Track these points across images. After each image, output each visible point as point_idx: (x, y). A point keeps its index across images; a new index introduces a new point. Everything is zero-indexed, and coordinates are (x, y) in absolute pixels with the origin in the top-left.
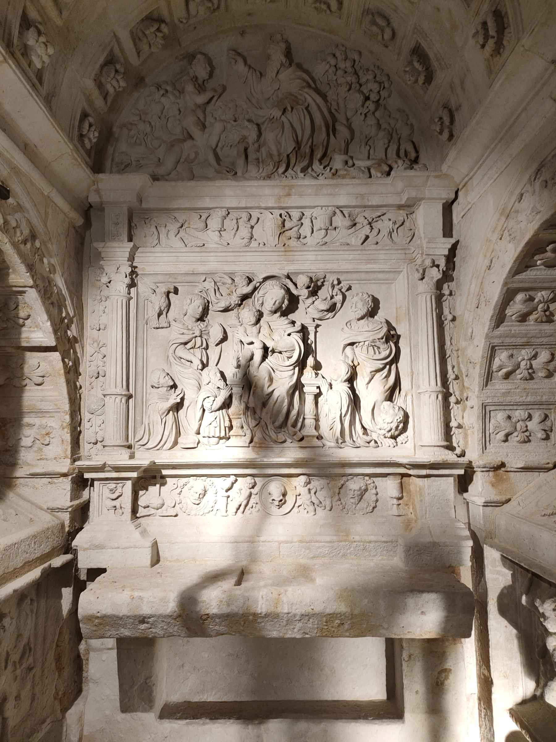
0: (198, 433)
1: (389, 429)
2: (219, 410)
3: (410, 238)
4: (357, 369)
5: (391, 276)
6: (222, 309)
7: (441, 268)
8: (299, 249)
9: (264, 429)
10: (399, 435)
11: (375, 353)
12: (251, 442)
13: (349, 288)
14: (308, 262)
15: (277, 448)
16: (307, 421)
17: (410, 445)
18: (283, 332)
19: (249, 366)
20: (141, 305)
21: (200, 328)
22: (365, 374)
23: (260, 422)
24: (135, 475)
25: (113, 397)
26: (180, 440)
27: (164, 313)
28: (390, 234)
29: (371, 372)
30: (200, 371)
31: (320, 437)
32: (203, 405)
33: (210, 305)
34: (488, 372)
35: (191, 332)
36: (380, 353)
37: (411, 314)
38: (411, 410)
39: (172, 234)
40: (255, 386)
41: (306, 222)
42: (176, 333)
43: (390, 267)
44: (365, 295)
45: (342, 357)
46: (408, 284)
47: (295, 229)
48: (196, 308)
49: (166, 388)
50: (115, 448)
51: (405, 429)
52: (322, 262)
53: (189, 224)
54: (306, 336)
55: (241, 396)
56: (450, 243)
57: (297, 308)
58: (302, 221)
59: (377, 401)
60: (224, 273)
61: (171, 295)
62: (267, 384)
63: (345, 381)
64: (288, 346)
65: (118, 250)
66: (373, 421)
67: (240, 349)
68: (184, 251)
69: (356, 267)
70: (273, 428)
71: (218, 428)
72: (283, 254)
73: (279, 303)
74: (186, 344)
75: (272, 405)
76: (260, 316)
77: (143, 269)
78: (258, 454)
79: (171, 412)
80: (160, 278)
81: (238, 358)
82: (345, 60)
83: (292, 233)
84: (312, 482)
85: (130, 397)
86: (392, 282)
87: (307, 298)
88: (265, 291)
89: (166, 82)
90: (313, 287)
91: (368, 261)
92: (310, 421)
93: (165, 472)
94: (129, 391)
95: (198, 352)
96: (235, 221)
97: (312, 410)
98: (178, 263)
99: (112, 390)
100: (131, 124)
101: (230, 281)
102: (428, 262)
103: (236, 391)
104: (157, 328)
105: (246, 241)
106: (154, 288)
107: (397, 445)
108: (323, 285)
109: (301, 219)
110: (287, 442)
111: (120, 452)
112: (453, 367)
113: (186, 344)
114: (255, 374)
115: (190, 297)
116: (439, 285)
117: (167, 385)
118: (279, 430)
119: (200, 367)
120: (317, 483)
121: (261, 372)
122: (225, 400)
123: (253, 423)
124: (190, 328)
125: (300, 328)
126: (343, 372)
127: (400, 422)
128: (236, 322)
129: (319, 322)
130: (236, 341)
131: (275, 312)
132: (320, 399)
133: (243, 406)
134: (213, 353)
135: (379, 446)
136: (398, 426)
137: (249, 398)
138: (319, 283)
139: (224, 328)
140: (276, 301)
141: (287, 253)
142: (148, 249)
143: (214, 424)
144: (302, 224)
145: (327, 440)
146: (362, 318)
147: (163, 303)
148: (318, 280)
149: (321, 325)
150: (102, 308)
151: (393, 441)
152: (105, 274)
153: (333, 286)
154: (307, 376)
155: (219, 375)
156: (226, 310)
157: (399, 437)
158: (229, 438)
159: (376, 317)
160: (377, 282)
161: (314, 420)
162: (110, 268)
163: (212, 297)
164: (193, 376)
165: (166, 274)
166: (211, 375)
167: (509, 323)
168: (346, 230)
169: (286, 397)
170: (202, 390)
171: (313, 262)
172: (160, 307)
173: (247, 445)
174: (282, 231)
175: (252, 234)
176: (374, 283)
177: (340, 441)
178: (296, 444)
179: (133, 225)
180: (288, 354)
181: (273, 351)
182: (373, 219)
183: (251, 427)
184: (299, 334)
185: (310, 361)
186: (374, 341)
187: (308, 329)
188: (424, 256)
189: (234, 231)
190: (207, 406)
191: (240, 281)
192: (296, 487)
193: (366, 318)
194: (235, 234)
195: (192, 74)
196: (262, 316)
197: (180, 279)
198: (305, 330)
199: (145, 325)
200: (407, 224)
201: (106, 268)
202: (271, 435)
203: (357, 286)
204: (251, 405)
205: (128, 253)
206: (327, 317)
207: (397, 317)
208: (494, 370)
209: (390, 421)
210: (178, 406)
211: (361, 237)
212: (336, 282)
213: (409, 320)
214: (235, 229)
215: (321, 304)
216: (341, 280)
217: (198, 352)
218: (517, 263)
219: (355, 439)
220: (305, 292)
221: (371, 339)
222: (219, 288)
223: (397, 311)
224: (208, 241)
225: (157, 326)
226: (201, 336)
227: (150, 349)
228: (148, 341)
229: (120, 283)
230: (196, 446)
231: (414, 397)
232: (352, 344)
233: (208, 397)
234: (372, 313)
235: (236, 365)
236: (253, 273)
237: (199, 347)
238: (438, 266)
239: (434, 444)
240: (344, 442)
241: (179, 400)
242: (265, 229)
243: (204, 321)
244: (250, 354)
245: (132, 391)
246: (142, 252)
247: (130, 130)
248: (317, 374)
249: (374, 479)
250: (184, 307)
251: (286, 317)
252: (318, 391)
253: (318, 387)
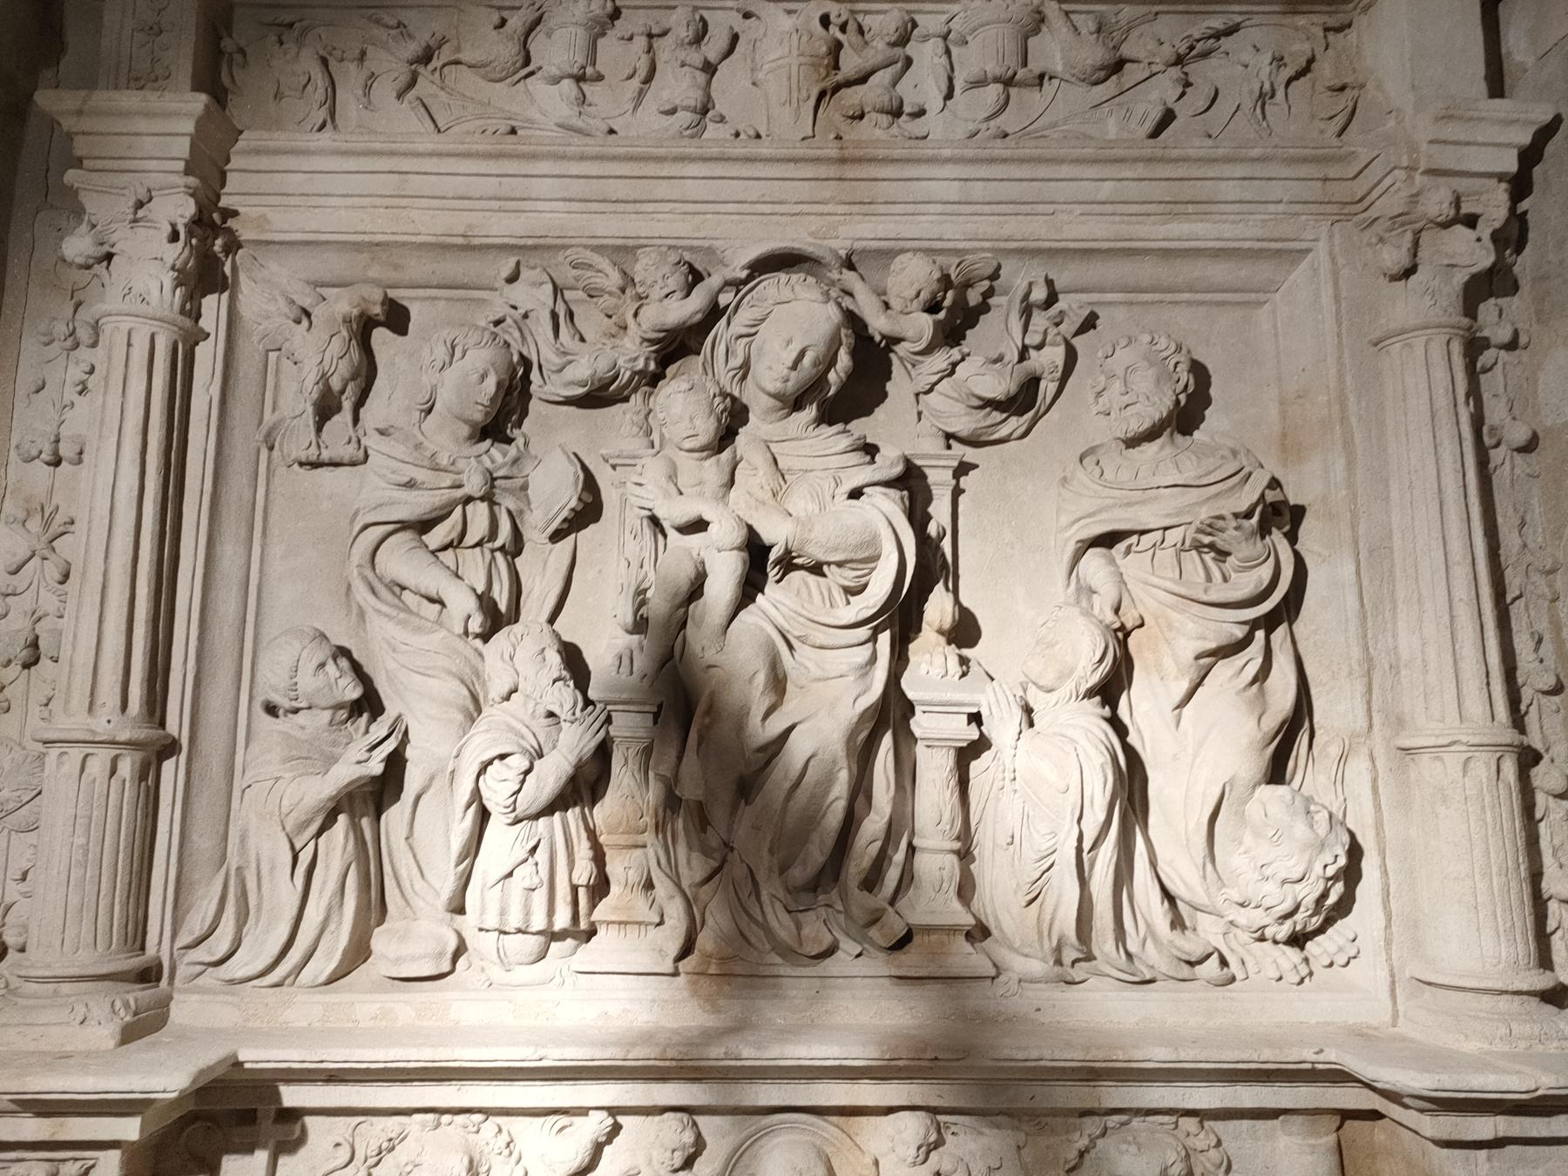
0: (460, 910)
1: (1287, 906)
2: (548, 810)
3: (1340, 121)
4: (1131, 641)
5: (1262, 271)
6: (581, 391)
8: (897, 153)
9: (744, 894)
10: (1321, 930)
11: (1209, 579)
12: (686, 950)
13: (1089, 323)
14: (930, 211)
15: (798, 982)
16: (923, 862)
17: (1369, 974)
18: (828, 485)
19: (685, 623)
20: (247, 366)
21: (488, 464)
22: (1168, 661)
23: (724, 861)
24: (129, 1129)
25: (76, 753)
26: (380, 941)
28: (1264, 97)
29: (1198, 658)
30: (478, 643)
31: (980, 933)
32: (476, 794)
33: (534, 375)
35: (448, 480)
37: (1354, 420)
38: (1369, 819)
39: (385, 90)
40: (711, 709)
41: (927, 54)
42: (380, 489)
43: (1259, 233)
46: (1337, 298)
47: (881, 78)
48: (470, 382)
49: (327, 715)
50: (66, 988)
51: (1345, 906)
52: (987, 209)
53: (458, 49)
54: (919, 505)
55: (647, 752)
56: (1527, 123)
57: (884, 396)
58: (910, 49)
59: (1232, 781)
60: (599, 249)
61: (380, 336)
62: (759, 705)
63: (1090, 694)
64: (853, 540)
65: (142, 125)
66: (1209, 867)
67: (648, 554)
68: (430, 147)
69: (1125, 230)
70: (781, 894)
71: (540, 897)
72: (832, 171)
73: (816, 364)
74: (423, 526)
75: (782, 796)
76: (733, 420)
77: (262, 221)
78: (716, 1010)
79: (342, 819)
80: (336, 264)
81: (641, 592)
83: (874, 92)
84: (949, 1138)
85: (170, 748)
86: (1262, 297)
87: (927, 351)
88: (756, 313)
90: (950, 309)
91: (1174, 208)
92: (936, 864)
93: (292, 1096)
94: (162, 724)
95: (474, 566)
96: (640, 42)
97: (946, 817)
98: (404, 202)
99: (71, 721)
103: (628, 726)
104: (316, 465)
105: (684, 118)
106: (306, 302)
107: (1311, 974)
108: (984, 308)
109: (903, 40)
110: (839, 954)
111: (81, 1011)
113: (423, 526)
114: (710, 656)
115: (447, 334)
117: (332, 702)
118: (806, 898)
119: (476, 625)
120: (972, 1146)
121: (736, 649)
122: (579, 767)
123: (693, 868)
125: (898, 469)
126: (1086, 658)
127: (1335, 878)
128: (636, 444)
130: (635, 518)
132: (975, 766)
133: (653, 794)
134: (541, 569)
135: (1233, 979)
136: (1324, 895)
137: (680, 758)
138: (973, 297)
139: (584, 468)
140: (802, 354)
141: (851, 171)
142: (279, 139)
143: (524, 876)
144: (909, 62)
145: (1016, 951)
146: (1151, 435)
147: (338, 361)
148: (968, 285)
149: (975, 466)
150: (76, 373)
151: (1293, 954)
152: (84, 227)
153: (1027, 312)
154: (924, 668)
155: (554, 659)
156: (598, 397)
157: (1319, 938)
158: (591, 933)
159: (1196, 433)
160: (1199, 297)
161: (954, 859)
162: (105, 205)
164: (442, 662)
165: (357, 247)
166: (523, 658)
168: (1082, 89)
169: (843, 762)
170: (482, 723)
171: (949, 208)
172: (324, 378)
173: (668, 967)
174: (828, 84)
175: (709, 97)
176: (1189, 303)
177: (1069, 955)
178: (876, 964)
179: (227, 44)
180: (848, 577)
181: (788, 564)
182: (1192, 48)
183: (685, 884)
184: (894, 493)
185: (938, 609)
186: (1211, 528)
187: (925, 477)
188: (1418, 178)
189: (636, 83)
190: (497, 792)
191: (652, 271)
192: (876, 1163)
193: (1167, 433)
194: (641, 94)
196: (745, 421)
197: (417, 268)
198: (913, 482)
199: (264, 453)
200: (1325, 70)
201: (90, 202)
202: (774, 923)
203: (1120, 314)
204: (690, 790)
205: (187, 141)
206: (1003, 432)
207: (1284, 435)
209: (1298, 876)
210: (383, 789)
211: (1145, 116)
212: (1039, 294)
213: (1348, 443)
214: (642, 72)
215: (983, 370)
216: (1058, 285)
217: (474, 566)
219: (1133, 946)
221: (1204, 514)
222: (571, 315)
223: (1283, 415)
224: (531, 121)
225: (312, 454)
226: (489, 498)
227: (276, 550)
228: (273, 519)
229: (147, 271)
230: (446, 967)
231: (1379, 764)
232: (1108, 540)
233: (502, 757)
234: (1185, 417)
235: (629, 619)
236: (710, 251)
237: (479, 544)
239: (1499, 985)
240: (1089, 957)
241: (376, 767)
242: (761, 75)
243: (510, 441)
244: (686, 573)
245: (176, 723)
246: (258, 152)
249: (1219, 1126)
250: (425, 379)
251: (840, 427)
252: (973, 734)
253: (975, 718)
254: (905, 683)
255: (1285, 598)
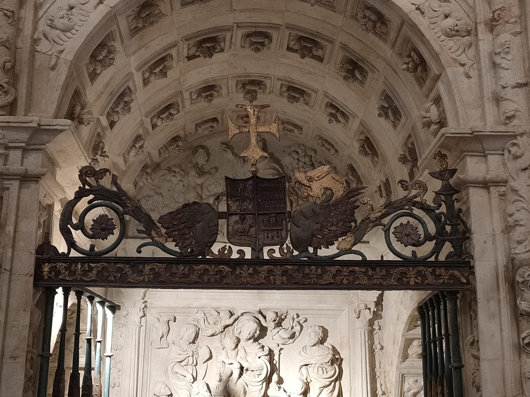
7: (372, 311)
11: (323, 373)
20: (148, 330)
27: (165, 336)
33: (200, 331)
34: (401, 392)
36: (327, 373)
44: (316, 328)
45: (299, 375)
60: (212, 308)
63: (301, 394)
74: (181, 362)
82: (305, 156)
87: (274, 329)
89: (175, 165)
95: (190, 368)
100: (149, 196)
101: (216, 314)
102: (362, 306)
108: (286, 317)
112: (381, 385)
113: (181, 362)
114: (234, 388)
115: (186, 326)
116: (371, 323)
119: (192, 381)
124: (185, 350)
125: (268, 352)
129: (282, 346)
131: (250, 339)
141: (260, 295)
146: (314, 345)
153: (294, 319)
155: (206, 387)
163: (202, 325)
164: (185, 387)
166: (199, 387)
167: (412, 359)
180: (258, 372)
184: (266, 357)
185: (275, 377)
186: (322, 364)
188: (359, 302)
195: (194, 161)
208: (405, 391)
212: (295, 317)
217: (190, 368)
218: (408, 325)
220: (273, 324)
221: (320, 362)
223: (341, 340)
226: (192, 356)
232: (307, 365)
234: (322, 341)
236: (234, 308)
238: (369, 309)
247: (147, 201)
248: (279, 388)
254: (268, 392)
255: (337, 377)
